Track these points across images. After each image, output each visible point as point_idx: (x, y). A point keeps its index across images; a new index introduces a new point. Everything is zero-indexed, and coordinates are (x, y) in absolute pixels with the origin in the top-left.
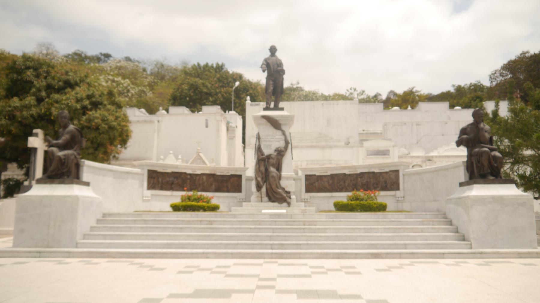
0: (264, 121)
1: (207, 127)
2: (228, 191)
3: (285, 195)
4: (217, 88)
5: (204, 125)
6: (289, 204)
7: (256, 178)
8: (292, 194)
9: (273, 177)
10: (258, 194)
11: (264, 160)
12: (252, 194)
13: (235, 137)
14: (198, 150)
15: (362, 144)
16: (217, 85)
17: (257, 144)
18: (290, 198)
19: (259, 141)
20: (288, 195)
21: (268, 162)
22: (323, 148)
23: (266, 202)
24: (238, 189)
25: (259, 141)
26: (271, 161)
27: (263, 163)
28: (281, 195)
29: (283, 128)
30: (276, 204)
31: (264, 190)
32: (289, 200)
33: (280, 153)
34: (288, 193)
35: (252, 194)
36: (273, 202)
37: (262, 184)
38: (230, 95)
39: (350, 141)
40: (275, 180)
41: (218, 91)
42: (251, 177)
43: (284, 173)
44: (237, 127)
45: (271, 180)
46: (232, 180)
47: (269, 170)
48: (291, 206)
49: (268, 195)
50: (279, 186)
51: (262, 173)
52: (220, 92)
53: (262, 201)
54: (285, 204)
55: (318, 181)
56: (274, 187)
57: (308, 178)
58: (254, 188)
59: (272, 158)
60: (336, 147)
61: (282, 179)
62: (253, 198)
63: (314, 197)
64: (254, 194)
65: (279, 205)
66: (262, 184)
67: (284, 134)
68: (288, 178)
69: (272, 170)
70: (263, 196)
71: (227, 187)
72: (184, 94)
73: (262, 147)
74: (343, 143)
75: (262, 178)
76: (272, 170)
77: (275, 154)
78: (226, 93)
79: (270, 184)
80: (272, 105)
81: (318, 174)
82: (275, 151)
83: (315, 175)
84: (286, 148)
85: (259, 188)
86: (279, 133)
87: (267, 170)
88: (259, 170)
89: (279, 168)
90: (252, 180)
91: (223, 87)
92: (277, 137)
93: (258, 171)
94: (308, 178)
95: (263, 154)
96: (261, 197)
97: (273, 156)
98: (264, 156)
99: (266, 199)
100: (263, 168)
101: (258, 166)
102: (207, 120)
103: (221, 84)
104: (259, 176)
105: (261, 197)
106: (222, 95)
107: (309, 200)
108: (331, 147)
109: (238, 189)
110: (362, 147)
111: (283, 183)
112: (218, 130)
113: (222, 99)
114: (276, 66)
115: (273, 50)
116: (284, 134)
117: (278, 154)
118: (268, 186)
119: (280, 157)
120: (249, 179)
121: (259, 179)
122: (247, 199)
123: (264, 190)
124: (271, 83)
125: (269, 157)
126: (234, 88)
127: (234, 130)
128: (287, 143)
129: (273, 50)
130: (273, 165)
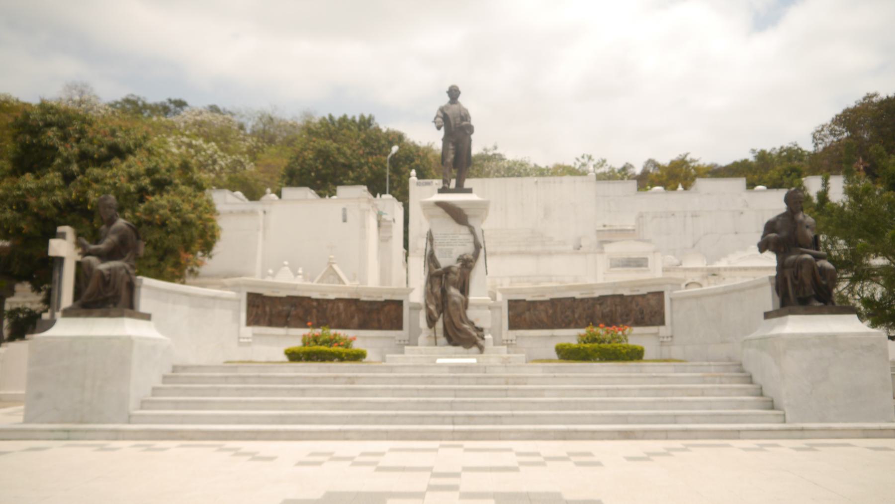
0: (440, 210)
1: (345, 221)
2: (380, 328)
3: (475, 334)
4: (362, 156)
5: (340, 218)
6: (481, 349)
7: (427, 306)
8: (486, 331)
9: (455, 303)
10: (431, 332)
11: (439, 275)
12: (420, 331)
13: (391, 237)
14: (330, 259)
15: (603, 248)
16: (361, 152)
17: (429, 249)
18: (483, 338)
19: (432, 245)
20: (480, 333)
21: (446, 278)
22: (537, 254)
23: (444, 345)
24: (397, 324)
25: (432, 245)
26: (452, 277)
27: (437, 280)
28: (469, 334)
29: (472, 222)
30: (460, 349)
31: (439, 325)
32: (481, 342)
33: (467, 264)
34: (480, 330)
35: (420, 331)
36: (455, 345)
37: (436, 315)
38: (384, 167)
39: (583, 244)
40: (458, 309)
41: (363, 161)
42: (418, 304)
43: (473, 298)
44: (394, 220)
45: (452, 308)
46: (386, 309)
47: (449, 292)
48: (485, 351)
49: (446, 334)
50: (464, 319)
51: (436, 298)
52: (367, 163)
53: (436, 344)
54: (475, 349)
55: (529, 310)
56: (456, 320)
57: (513, 305)
58: (423, 323)
59: (453, 272)
60: (558, 253)
61: (470, 307)
62: (422, 339)
63: (523, 337)
64: (424, 332)
65: (466, 351)
66: (436, 315)
67: (472, 232)
68: (479, 306)
69: (454, 291)
70: (438, 335)
71: (379, 321)
72: (306, 167)
73: (437, 254)
74: (570, 247)
75: (437, 306)
76: (454, 291)
77: (459, 265)
78: (376, 164)
79: (450, 316)
80: (453, 184)
81: (529, 298)
82: (458, 260)
83: (524, 300)
84: (476, 255)
85: (431, 322)
86: (464, 230)
87: (444, 292)
88: (432, 292)
89: (464, 289)
90: (420, 309)
91: (371, 154)
92: (461, 237)
93: (429, 293)
94: (513, 305)
95: (437, 266)
96: (436, 338)
97: (455, 269)
98: (439, 270)
99: (443, 340)
100: (437, 290)
101: (429, 285)
102: (344, 210)
103: (367, 150)
104: (432, 303)
105: (436, 338)
106: (370, 168)
107: (514, 342)
108: (550, 254)
109: (397, 324)
110: (602, 252)
111: (471, 314)
112: (363, 226)
113: (369, 175)
114: (459, 119)
115: (454, 93)
116: (472, 232)
117: (462, 265)
118: (447, 320)
119: (465, 271)
120: (415, 308)
121: (432, 307)
122: (412, 341)
123: (439, 325)
124: (451, 147)
125: (448, 270)
126: (389, 156)
127: (391, 226)
128: (478, 247)
129: (454, 93)
130: (455, 285)
